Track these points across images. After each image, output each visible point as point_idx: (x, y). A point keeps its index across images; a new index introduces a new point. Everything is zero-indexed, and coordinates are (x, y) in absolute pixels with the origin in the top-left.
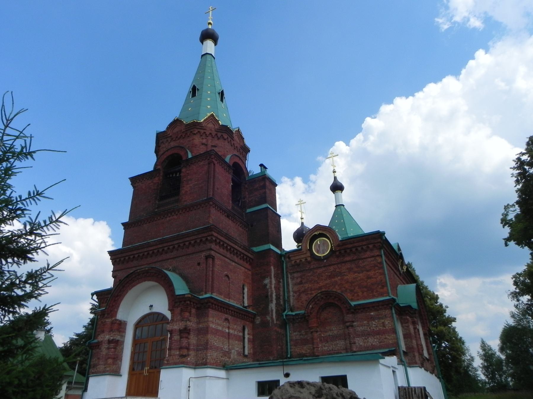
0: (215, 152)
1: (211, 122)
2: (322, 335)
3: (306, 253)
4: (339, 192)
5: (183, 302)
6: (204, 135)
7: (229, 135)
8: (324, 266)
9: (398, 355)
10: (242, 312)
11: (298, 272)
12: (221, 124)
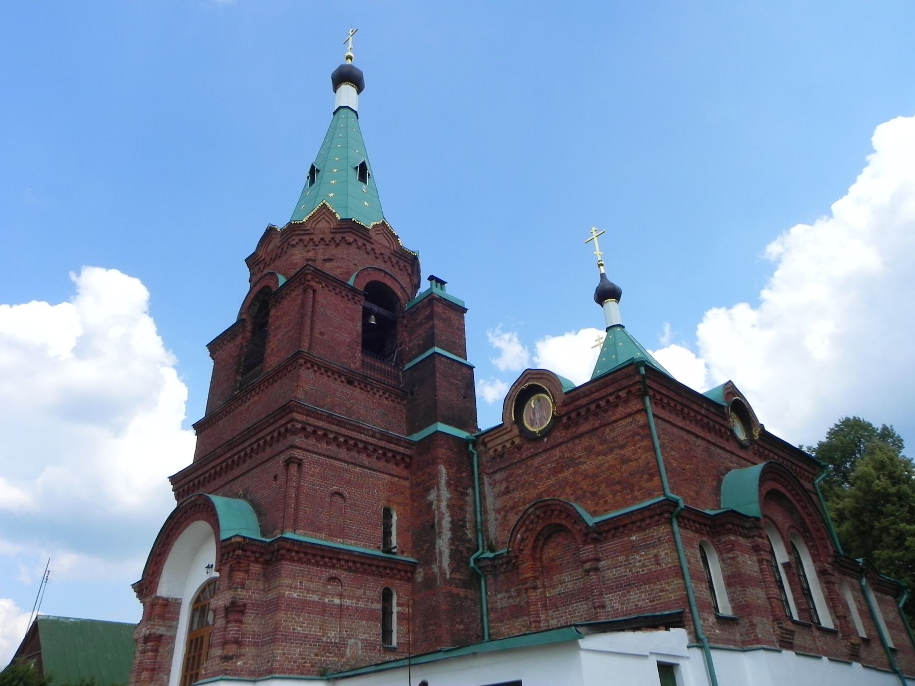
0: (312, 269)
1: (323, 218)
2: (547, 595)
3: (511, 431)
4: (611, 303)
5: (258, 555)
6: (311, 243)
7: (359, 234)
8: (545, 451)
9: (689, 625)
10: (375, 563)
11: (500, 470)
12: (339, 218)
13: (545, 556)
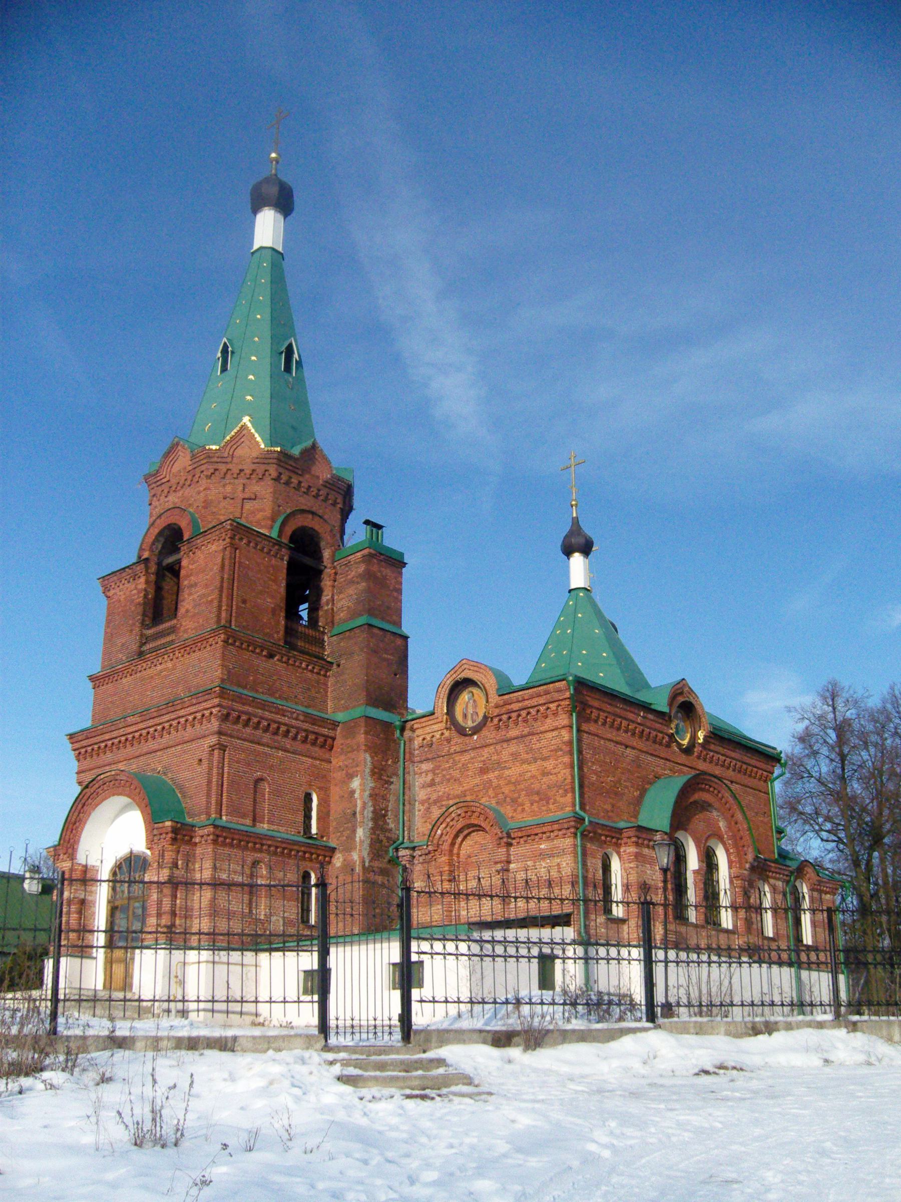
11: (427, 760)
13: (462, 852)
